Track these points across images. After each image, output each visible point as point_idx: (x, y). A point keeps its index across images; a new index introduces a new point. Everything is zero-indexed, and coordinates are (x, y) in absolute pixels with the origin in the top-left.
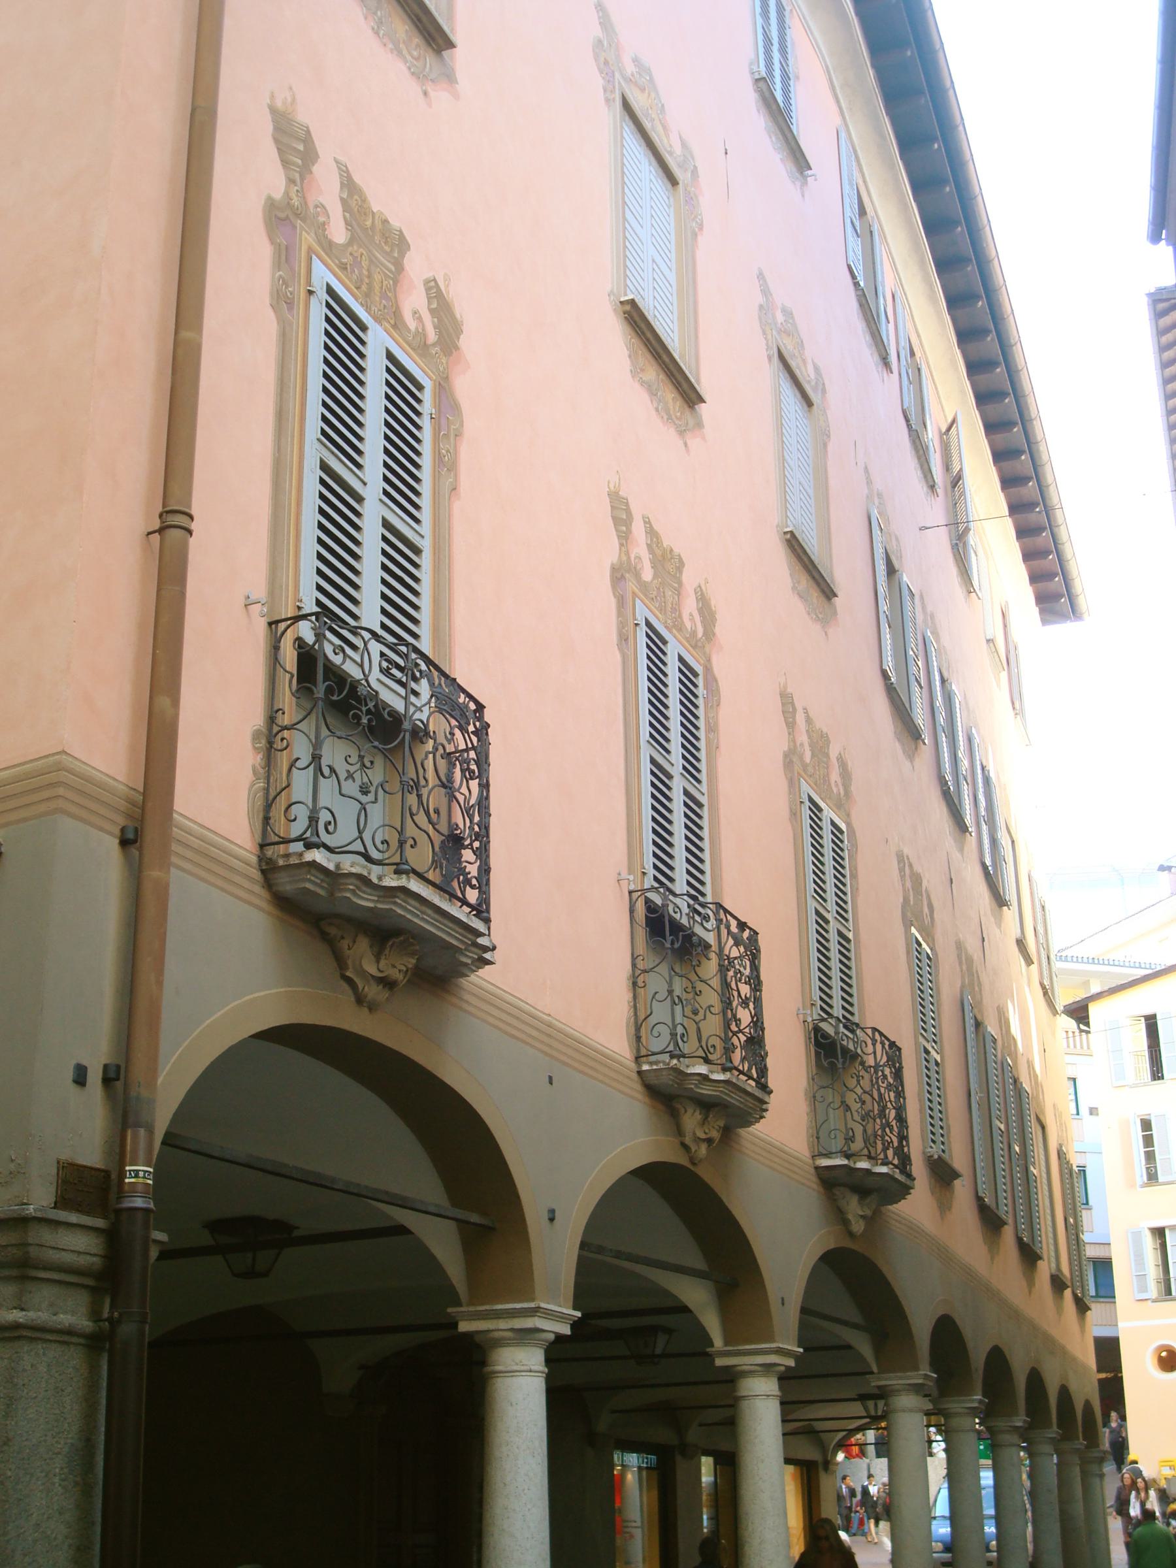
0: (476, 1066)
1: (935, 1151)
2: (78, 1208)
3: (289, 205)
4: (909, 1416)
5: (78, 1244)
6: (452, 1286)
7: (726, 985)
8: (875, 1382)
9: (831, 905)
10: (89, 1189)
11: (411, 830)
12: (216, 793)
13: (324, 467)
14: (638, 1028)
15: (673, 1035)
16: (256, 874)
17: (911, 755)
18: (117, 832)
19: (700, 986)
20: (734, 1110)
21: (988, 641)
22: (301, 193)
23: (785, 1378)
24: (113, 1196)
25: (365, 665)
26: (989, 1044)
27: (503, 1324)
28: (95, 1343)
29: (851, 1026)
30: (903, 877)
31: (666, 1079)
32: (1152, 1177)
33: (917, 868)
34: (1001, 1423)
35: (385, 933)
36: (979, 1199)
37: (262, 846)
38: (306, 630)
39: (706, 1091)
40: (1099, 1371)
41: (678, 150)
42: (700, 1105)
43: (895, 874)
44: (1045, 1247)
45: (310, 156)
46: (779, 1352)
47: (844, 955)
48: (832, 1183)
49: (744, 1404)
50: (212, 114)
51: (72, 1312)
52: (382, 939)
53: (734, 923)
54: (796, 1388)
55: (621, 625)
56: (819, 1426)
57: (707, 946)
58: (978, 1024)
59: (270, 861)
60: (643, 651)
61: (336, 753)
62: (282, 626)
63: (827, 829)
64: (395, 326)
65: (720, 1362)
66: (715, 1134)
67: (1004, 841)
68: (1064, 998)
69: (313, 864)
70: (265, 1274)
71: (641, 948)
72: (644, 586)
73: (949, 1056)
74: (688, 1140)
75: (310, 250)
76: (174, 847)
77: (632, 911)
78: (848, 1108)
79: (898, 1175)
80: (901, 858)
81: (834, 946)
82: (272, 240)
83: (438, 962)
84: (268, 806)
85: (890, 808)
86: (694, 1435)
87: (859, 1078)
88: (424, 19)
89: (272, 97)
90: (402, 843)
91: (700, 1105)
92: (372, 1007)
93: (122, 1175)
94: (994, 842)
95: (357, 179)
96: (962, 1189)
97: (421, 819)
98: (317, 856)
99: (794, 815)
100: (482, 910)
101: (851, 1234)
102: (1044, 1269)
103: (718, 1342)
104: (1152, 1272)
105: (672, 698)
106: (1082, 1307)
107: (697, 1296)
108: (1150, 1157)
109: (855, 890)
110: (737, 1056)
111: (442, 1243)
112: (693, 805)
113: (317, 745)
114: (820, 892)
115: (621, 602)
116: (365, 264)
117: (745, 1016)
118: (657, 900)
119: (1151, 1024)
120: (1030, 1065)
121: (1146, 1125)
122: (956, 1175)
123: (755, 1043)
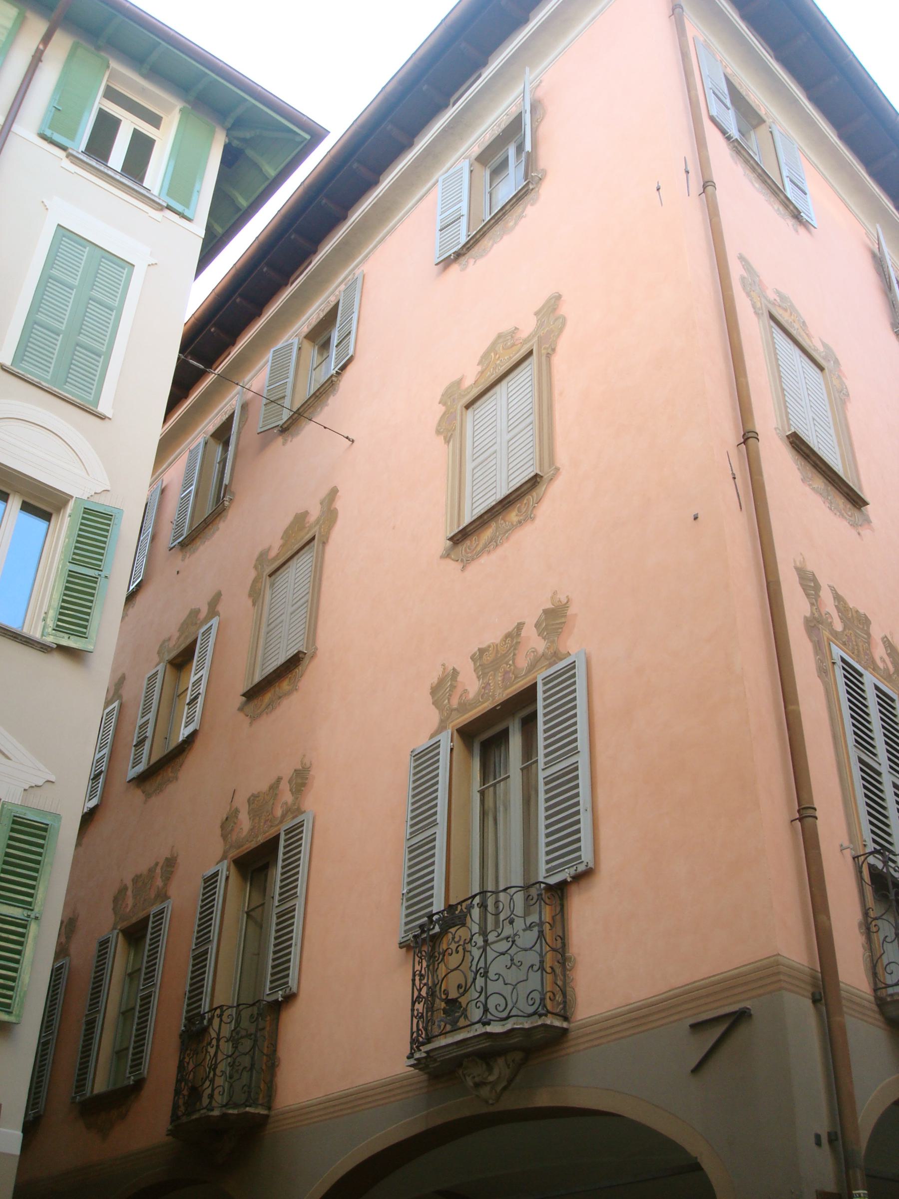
3: (815, 618)
12: (853, 973)
13: (861, 761)
16: (875, 1008)
18: (810, 996)
22: (818, 609)
37: (875, 990)
41: (821, 349)
45: (817, 588)
50: (778, 583)
60: (841, 681)
62: (862, 858)
64: (874, 669)
75: (828, 639)
82: (811, 640)
88: (851, 494)
89: (795, 561)
95: (840, 593)
116: (853, 638)
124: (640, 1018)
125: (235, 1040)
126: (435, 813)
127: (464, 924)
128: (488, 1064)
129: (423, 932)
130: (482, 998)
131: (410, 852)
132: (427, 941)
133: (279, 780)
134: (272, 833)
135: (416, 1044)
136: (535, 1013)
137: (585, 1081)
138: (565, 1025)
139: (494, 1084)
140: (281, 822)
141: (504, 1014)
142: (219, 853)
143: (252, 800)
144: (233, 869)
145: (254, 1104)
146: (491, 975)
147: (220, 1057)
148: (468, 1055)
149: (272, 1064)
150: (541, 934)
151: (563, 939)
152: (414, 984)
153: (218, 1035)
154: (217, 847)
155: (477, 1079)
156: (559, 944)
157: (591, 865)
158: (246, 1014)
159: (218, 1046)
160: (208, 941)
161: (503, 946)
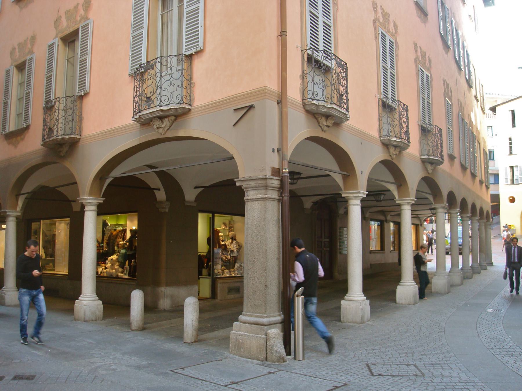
0: (345, 141)
1: (450, 153)
2: (275, 176)
4: (442, 215)
5: (275, 182)
6: (339, 185)
7: (400, 119)
8: (433, 206)
9: (426, 95)
10: (276, 172)
11: (333, 94)
12: (294, 93)
13: (311, 12)
14: (380, 130)
15: (388, 132)
16: (302, 106)
17: (447, 53)
19: (394, 120)
20: (400, 148)
21: (469, 16)
23: (412, 205)
24: (281, 173)
25: (320, 56)
26: (465, 124)
27: (351, 195)
28: (279, 200)
29: (430, 125)
30: (444, 85)
31: (387, 142)
32: (511, 153)
33: (448, 82)
34: (464, 215)
35: (327, 116)
36: (461, 163)
38: (310, 52)
39: (396, 144)
40: (492, 202)
42: (393, 147)
43: (442, 85)
44: (478, 174)
46: (411, 200)
47: (327, 34)
48: (424, 161)
49: (403, 211)
51: (275, 195)
52: (326, 117)
53: (402, 104)
54: (414, 207)
55: (375, 34)
56: (419, 216)
57: (396, 109)
58: (463, 120)
59: (304, 103)
61: (317, 79)
63: (425, 76)
65: (397, 202)
66: (397, 153)
67: (472, 70)
68: (488, 105)
69: (314, 104)
70: (295, 184)
71: (380, 112)
72: (380, 23)
73: (455, 129)
74: (391, 154)
76: (288, 103)
77: (379, 103)
78: (429, 144)
79: (440, 159)
80: (444, 80)
81: (426, 105)
83: (337, 121)
84: (303, 91)
85: (441, 67)
86: (389, 218)
87: (431, 137)
90: (331, 97)
91: (393, 147)
92: (325, 132)
93: (282, 169)
94: (469, 71)
96: (457, 161)
97: (335, 91)
98: (314, 102)
99: (417, 74)
100: (347, 110)
101: (428, 173)
102: (478, 179)
103: (397, 197)
104: (509, 178)
105: (388, 50)
106: (487, 188)
107: (393, 188)
108: (511, 148)
109: (432, 90)
110: (403, 136)
111: (338, 179)
112: (327, 26)
113: (313, 78)
114: (423, 92)
115: (375, 28)
117: (404, 126)
118: (384, 100)
119: (513, 112)
120: (477, 128)
121: (510, 139)
122: (455, 158)
123: (407, 132)
124: (216, 107)
125: (65, 110)
126: (143, 23)
127: (153, 69)
128: (162, 121)
129: (138, 71)
130: (159, 97)
131: (133, 39)
132: (140, 74)
133: (78, 4)
134: (75, 28)
135: (135, 113)
136: (179, 103)
137: (193, 127)
138: (190, 107)
139: (164, 128)
140: (80, 23)
141: (168, 103)
142: (54, 36)
143: (67, 12)
144: (60, 41)
145: (75, 134)
146: (163, 88)
147: (60, 116)
148: (154, 117)
149: (81, 120)
150: (182, 73)
151: (191, 76)
152: (134, 91)
153: (59, 108)
154: (53, 32)
155: (158, 126)
156: (189, 78)
157: (202, 48)
158: (69, 100)
159: (59, 113)
160: (52, 71)
161: (168, 77)
